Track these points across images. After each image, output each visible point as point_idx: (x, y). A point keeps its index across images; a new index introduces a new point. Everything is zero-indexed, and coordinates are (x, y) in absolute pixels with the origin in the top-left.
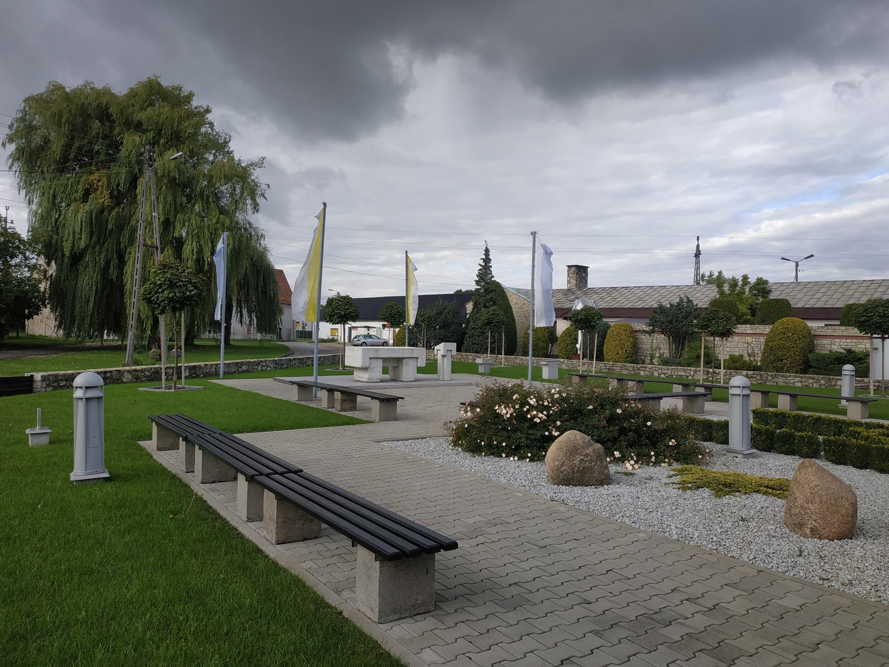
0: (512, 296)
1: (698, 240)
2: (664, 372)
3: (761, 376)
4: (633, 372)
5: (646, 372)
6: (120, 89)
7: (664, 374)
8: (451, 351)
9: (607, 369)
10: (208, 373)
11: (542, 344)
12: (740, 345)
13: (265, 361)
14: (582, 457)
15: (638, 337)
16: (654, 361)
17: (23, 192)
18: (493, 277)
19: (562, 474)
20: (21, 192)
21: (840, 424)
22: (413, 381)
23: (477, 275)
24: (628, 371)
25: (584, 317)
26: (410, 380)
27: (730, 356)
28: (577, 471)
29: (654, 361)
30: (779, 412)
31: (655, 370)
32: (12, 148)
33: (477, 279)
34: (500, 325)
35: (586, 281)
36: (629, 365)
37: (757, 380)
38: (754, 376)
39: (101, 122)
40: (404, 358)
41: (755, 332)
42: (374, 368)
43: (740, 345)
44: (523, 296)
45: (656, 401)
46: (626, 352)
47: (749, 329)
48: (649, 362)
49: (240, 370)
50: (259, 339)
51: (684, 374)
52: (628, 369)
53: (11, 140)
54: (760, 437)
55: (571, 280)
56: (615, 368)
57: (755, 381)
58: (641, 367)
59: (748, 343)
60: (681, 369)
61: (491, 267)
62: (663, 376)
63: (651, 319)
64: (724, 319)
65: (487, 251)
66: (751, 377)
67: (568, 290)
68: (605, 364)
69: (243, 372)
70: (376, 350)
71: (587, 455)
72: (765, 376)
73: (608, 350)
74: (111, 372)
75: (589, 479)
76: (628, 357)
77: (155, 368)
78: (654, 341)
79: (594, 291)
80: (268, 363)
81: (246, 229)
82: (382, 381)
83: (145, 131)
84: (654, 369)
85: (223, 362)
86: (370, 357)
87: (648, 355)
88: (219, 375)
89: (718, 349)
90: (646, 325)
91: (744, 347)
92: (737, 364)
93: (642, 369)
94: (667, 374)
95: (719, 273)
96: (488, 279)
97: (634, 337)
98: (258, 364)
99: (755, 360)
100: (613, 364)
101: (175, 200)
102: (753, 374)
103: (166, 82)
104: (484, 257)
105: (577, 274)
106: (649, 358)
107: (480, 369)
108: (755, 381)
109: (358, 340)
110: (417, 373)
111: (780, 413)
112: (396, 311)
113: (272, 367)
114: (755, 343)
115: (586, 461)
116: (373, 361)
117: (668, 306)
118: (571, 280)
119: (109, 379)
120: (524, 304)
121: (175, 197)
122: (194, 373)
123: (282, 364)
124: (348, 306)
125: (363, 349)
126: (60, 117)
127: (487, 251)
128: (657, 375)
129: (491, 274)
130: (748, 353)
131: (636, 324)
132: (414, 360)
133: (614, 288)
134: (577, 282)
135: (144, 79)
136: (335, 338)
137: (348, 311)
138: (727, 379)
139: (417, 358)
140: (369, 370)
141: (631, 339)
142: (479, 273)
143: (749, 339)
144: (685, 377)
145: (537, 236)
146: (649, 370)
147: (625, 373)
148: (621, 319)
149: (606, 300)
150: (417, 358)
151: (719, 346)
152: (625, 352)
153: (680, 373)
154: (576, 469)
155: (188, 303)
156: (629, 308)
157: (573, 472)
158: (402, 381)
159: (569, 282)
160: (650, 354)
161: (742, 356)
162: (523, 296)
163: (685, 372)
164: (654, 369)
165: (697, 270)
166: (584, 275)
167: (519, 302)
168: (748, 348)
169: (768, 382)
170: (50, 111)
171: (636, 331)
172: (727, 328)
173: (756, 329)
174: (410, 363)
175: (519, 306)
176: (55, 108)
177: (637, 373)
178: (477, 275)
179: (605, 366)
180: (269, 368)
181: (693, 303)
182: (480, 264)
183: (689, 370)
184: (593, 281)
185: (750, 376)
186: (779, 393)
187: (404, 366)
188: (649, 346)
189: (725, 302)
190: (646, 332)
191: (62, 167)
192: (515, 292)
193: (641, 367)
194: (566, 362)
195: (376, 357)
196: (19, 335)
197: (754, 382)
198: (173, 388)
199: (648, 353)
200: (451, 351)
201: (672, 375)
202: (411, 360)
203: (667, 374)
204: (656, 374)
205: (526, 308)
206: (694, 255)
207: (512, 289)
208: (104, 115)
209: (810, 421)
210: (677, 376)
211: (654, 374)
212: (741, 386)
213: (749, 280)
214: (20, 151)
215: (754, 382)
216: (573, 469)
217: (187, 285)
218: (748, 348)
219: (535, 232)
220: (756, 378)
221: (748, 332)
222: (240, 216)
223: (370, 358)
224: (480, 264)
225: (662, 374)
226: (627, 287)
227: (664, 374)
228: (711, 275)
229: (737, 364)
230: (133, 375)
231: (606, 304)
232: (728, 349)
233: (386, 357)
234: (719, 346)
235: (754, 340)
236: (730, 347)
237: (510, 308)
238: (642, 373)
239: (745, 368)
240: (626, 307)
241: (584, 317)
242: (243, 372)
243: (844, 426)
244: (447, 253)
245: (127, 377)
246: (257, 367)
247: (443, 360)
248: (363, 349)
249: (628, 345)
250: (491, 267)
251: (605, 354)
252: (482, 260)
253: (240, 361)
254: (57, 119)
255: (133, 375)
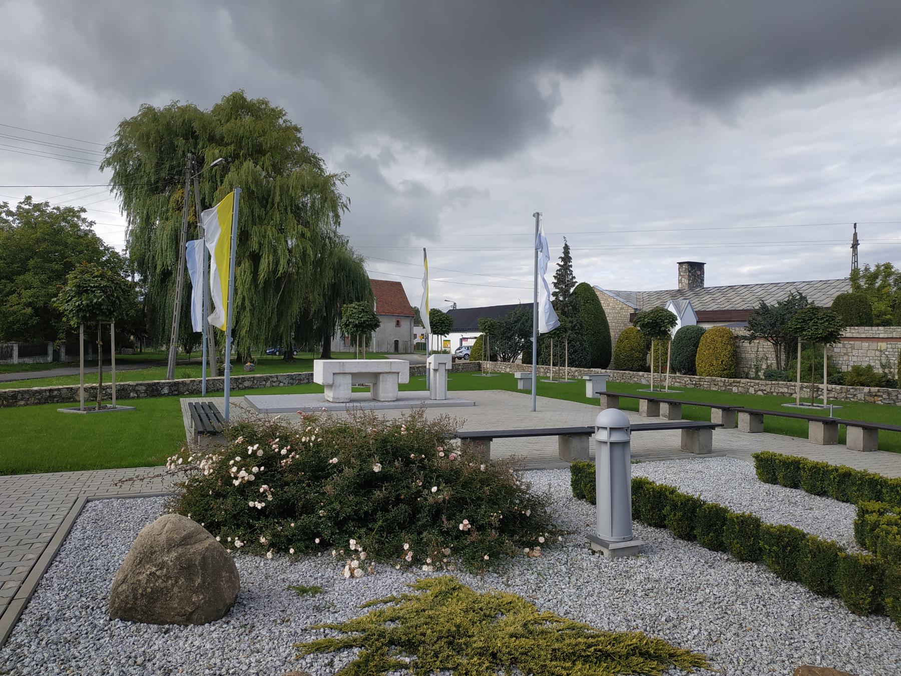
0: (609, 300)
1: (855, 228)
2: (762, 388)
3: (888, 393)
4: (724, 388)
5: (740, 388)
6: (206, 106)
7: (762, 390)
8: (445, 364)
9: (692, 384)
10: (195, 390)
11: (637, 354)
12: (871, 353)
13: (277, 377)
14: (154, 569)
15: (741, 344)
16: (760, 374)
17: (125, 213)
18: (574, 277)
19: (118, 598)
20: (124, 213)
21: (879, 487)
22: (394, 401)
23: (554, 276)
24: (717, 387)
25: (651, 321)
26: (389, 400)
27: (852, 367)
28: (142, 594)
29: (760, 374)
30: (790, 461)
31: (750, 386)
32: (109, 172)
33: (556, 281)
34: (560, 333)
35: (702, 280)
36: (719, 379)
37: (884, 399)
38: (879, 394)
39: (187, 139)
40: (380, 373)
41: (890, 336)
42: (340, 385)
43: (871, 353)
44: (621, 300)
45: (584, 438)
46: (722, 363)
47: (882, 332)
48: (754, 376)
49: (241, 386)
50: (374, 351)
51: (786, 391)
52: (718, 384)
53: (108, 162)
54: (675, 515)
55: (683, 279)
56: (702, 383)
57: (881, 400)
58: (734, 382)
59: (881, 351)
60: (783, 384)
61: (571, 266)
62: (760, 393)
63: (750, 322)
64: (825, 319)
65: (566, 249)
66: (876, 396)
67: (679, 290)
68: (690, 378)
69: (246, 388)
70: (342, 364)
71: (161, 566)
72: (894, 394)
73: (700, 361)
74: (59, 390)
75: (162, 611)
76: (725, 370)
77: (121, 385)
78: (760, 349)
79: (708, 291)
80: (280, 378)
81: (330, 238)
82: (352, 401)
83: (227, 145)
84: (749, 384)
85: (227, 377)
86: (334, 372)
87: (753, 366)
88: (201, 392)
89: (841, 359)
90: (745, 330)
91: (876, 356)
92: (863, 378)
93: (735, 384)
94: (765, 390)
95: (877, 266)
96: (568, 281)
97: (734, 345)
98: (266, 379)
99: (891, 372)
100: (700, 379)
101: (252, 212)
102: (879, 391)
103: (251, 96)
104: (563, 255)
105: (690, 272)
106: (754, 370)
107: (519, 385)
108: (881, 400)
109: (460, 352)
110: (399, 391)
111: (792, 462)
112: (438, 318)
113: (287, 383)
114: (891, 350)
115: (159, 577)
116: (338, 377)
117: (777, 305)
118: (683, 279)
119: (56, 397)
120: (622, 308)
121: (253, 209)
122: (176, 391)
123: (300, 380)
124: (362, 314)
125: (324, 363)
126: (148, 138)
127: (566, 249)
128: (753, 392)
129: (571, 274)
130: (881, 363)
131: (737, 329)
132: (393, 375)
133: (731, 287)
134: (690, 282)
135: (228, 93)
136: (448, 350)
137: (362, 319)
138: (843, 398)
139: (398, 373)
140: (333, 388)
141: (729, 347)
142: (557, 274)
143: (883, 345)
144: (787, 395)
145: (541, 218)
146: (743, 385)
147: (714, 389)
148: (730, 323)
149: (719, 301)
150: (398, 373)
151: (843, 354)
152: (720, 363)
153: (781, 390)
154: (140, 591)
155: (97, 313)
156: (743, 310)
157: (135, 598)
158: (379, 401)
159: (680, 282)
160: (755, 365)
161: (870, 368)
162: (621, 300)
163: (788, 388)
164: (749, 384)
165: (854, 263)
166: (699, 273)
167: (616, 306)
168: (881, 356)
169: (899, 402)
170: (138, 133)
171: (737, 337)
172: (828, 331)
173: (892, 333)
174: (388, 380)
175: (617, 311)
176: (144, 129)
177: (729, 389)
178: (554, 276)
179: (691, 380)
180: (282, 384)
181: (807, 301)
182: (558, 264)
183: (792, 386)
184: (710, 281)
185: (874, 394)
186: (847, 425)
187: (381, 383)
188: (753, 356)
189: (852, 298)
190: (745, 338)
191: (155, 189)
192: (611, 295)
193: (734, 382)
194: (646, 376)
195: (342, 372)
196: (143, 351)
197: (880, 402)
198: (97, 409)
199: (753, 364)
200: (445, 364)
201: (772, 393)
202: (390, 376)
203: (765, 390)
204: (752, 391)
205: (624, 314)
206: (851, 246)
207: (611, 291)
208: (190, 134)
209: (834, 478)
210: (777, 393)
211: (750, 391)
212: (609, 425)
213: (893, 270)
214: (117, 175)
215: (880, 402)
216: (135, 590)
217: (95, 290)
218: (881, 356)
219: (538, 214)
220: (881, 396)
221: (881, 336)
222: (322, 227)
223: (334, 374)
224: (558, 264)
225: (760, 390)
226: (747, 285)
227: (762, 390)
228: (867, 269)
229: (863, 378)
230: (90, 393)
231: (702, 307)
232: (855, 359)
233: (356, 372)
234: (843, 354)
235: (889, 346)
236: (858, 356)
237: (602, 312)
238: (735, 389)
239: (872, 384)
240: (741, 308)
241: (651, 321)
242: (246, 388)
243: (884, 491)
244: (594, 259)
245: (82, 395)
246: (264, 382)
247: (435, 376)
248: (324, 363)
249: (725, 355)
250: (571, 266)
251: (696, 366)
252: (561, 260)
253: (241, 376)
254: (144, 140)
255: (90, 393)
